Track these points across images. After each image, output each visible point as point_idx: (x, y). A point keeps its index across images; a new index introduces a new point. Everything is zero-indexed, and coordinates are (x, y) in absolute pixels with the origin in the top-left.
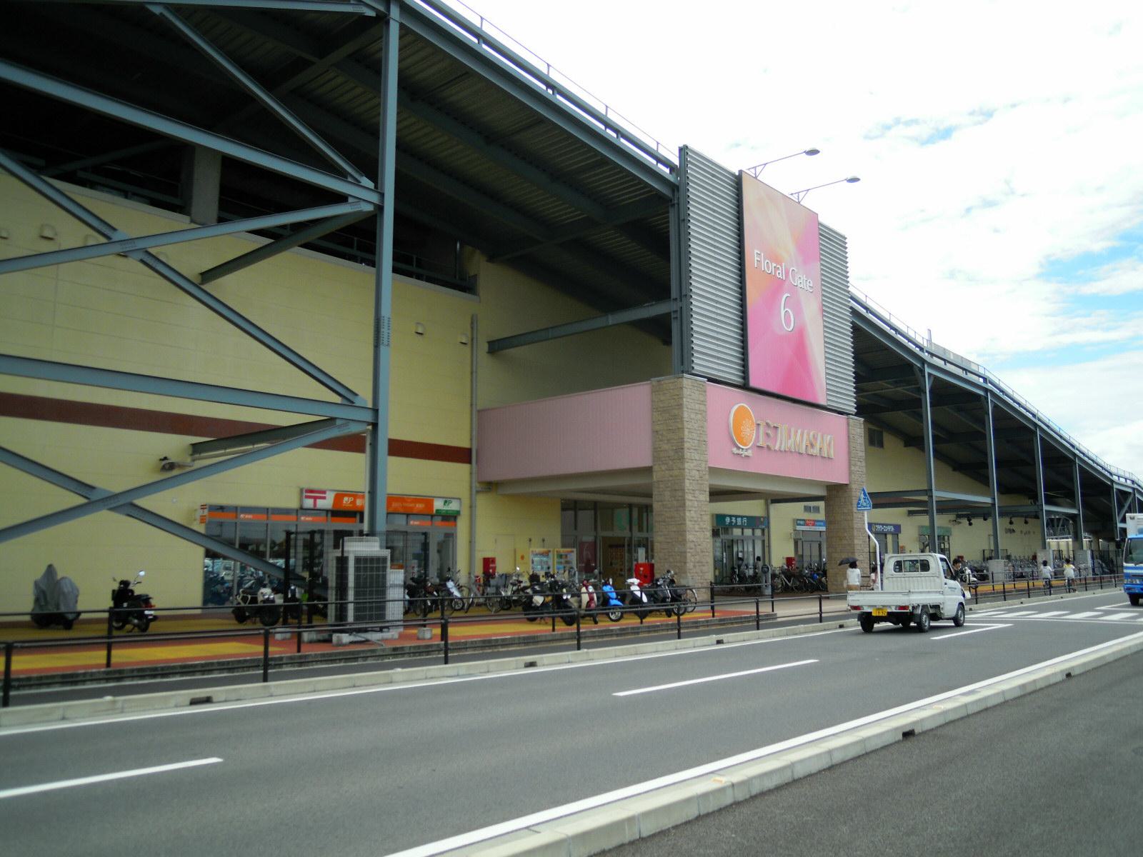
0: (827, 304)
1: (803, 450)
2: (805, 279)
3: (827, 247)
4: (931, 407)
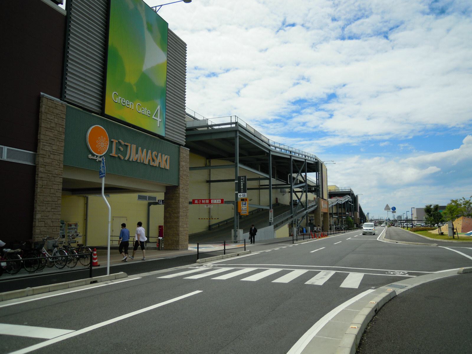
0: (169, 89)
1: (146, 162)
2: (146, 110)
3: (177, 120)
4: (239, 156)
